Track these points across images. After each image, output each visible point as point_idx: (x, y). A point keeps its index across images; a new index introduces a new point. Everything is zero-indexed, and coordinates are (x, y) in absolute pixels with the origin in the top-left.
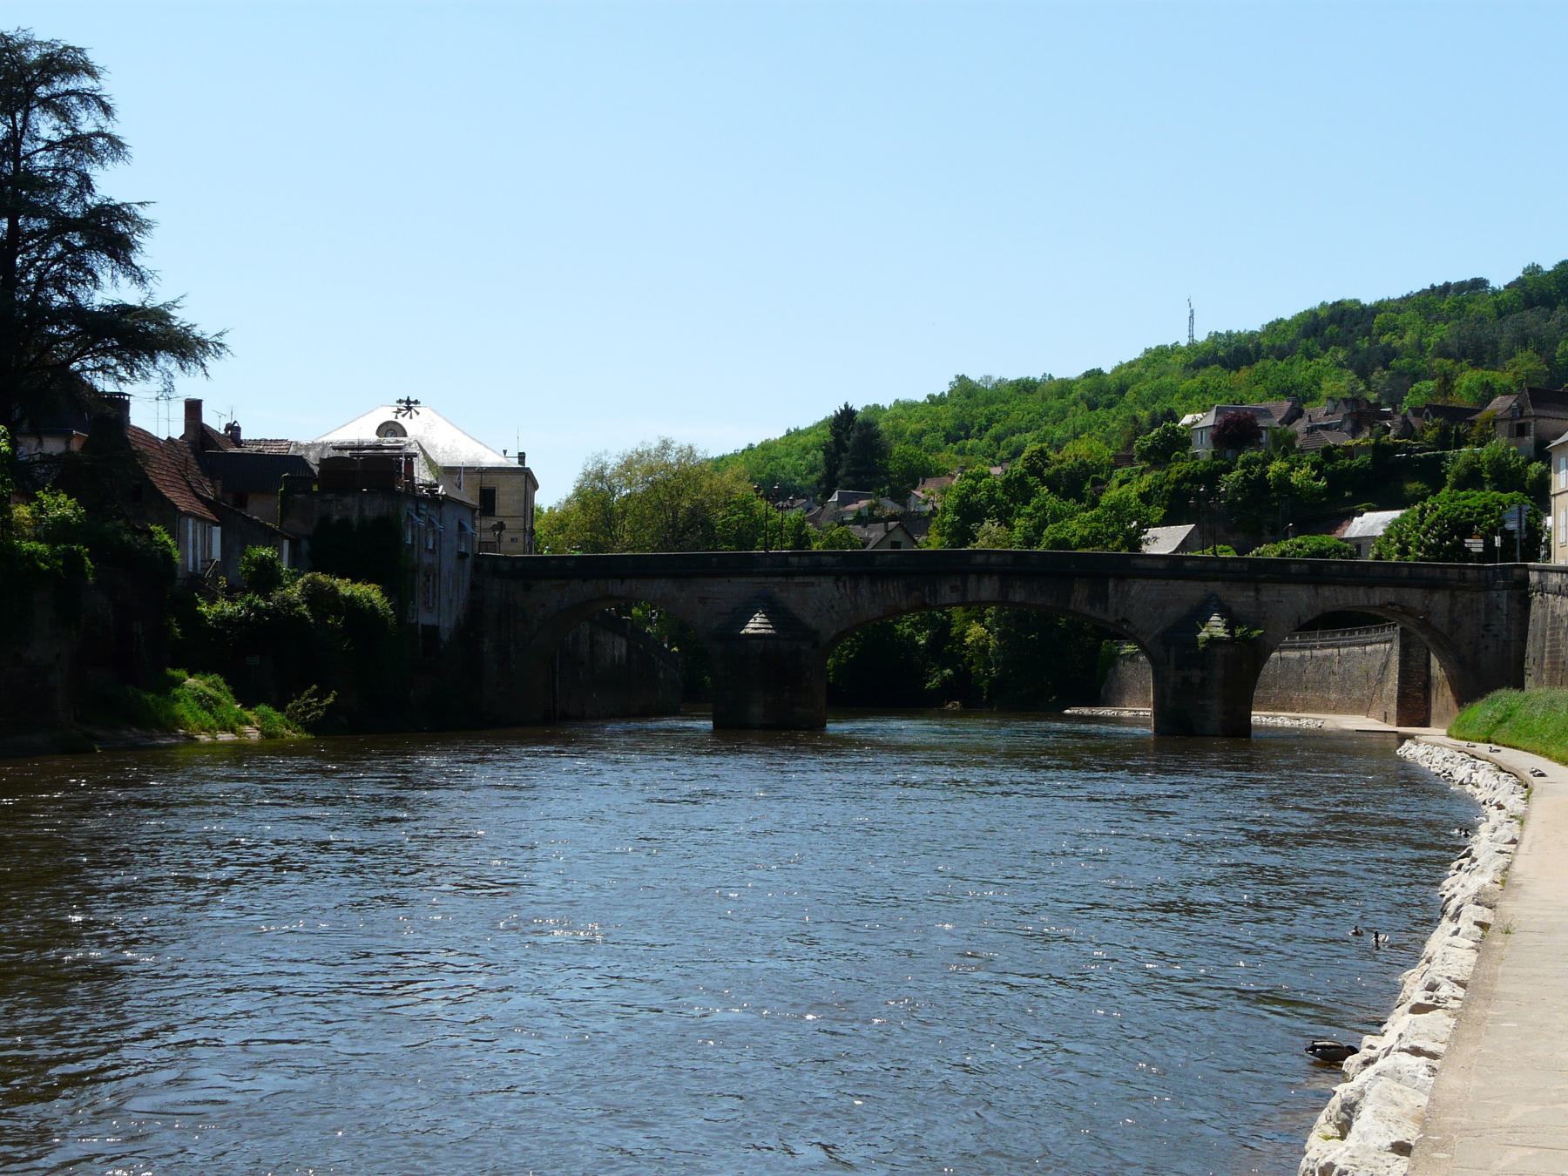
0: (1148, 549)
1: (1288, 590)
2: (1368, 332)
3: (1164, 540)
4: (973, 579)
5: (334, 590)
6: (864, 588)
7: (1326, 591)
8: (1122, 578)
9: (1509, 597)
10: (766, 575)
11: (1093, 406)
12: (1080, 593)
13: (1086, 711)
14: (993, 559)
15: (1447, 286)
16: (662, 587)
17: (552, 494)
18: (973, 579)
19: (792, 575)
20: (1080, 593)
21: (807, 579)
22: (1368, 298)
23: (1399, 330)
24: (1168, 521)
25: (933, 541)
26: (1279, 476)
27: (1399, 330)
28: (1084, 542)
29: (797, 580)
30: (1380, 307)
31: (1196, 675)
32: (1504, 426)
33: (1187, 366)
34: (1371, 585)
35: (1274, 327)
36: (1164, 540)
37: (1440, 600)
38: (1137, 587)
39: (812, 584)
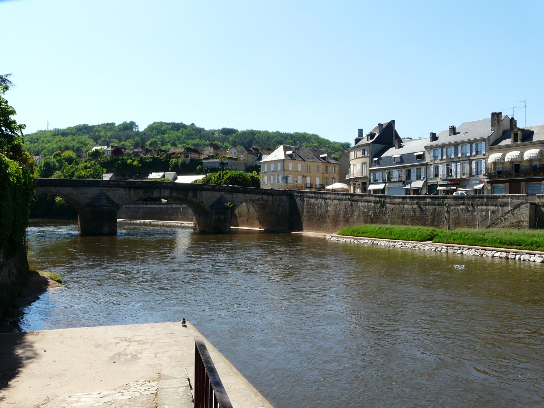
0: (104, 179)
1: (239, 195)
2: (93, 132)
3: (107, 177)
4: (163, 190)
5: (324, 240)
6: (132, 191)
7: (247, 195)
8: (201, 190)
9: (287, 198)
10: (103, 187)
11: (31, 142)
12: (191, 194)
13: (148, 221)
14: (168, 184)
15: (108, 123)
16: (68, 190)
17: (116, 125)
18: (163, 190)
19: (111, 187)
20: (191, 194)
21: (115, 189)
22: (90, 124)
23: (100, 132)
24: (107, 172)
25: (36, 175)
26: (130, 163)
27: (100, 132)
28: (88, 177)
29: (113, 188)
30: (93, 127)
31: (222, 217)
32: (183, 155)
33: (52, 135)
34: (256, 194)
35: (69, 128)
36: (107, 177)
37: (270, 198)
38: (204, 193)
39: (117, 190)
